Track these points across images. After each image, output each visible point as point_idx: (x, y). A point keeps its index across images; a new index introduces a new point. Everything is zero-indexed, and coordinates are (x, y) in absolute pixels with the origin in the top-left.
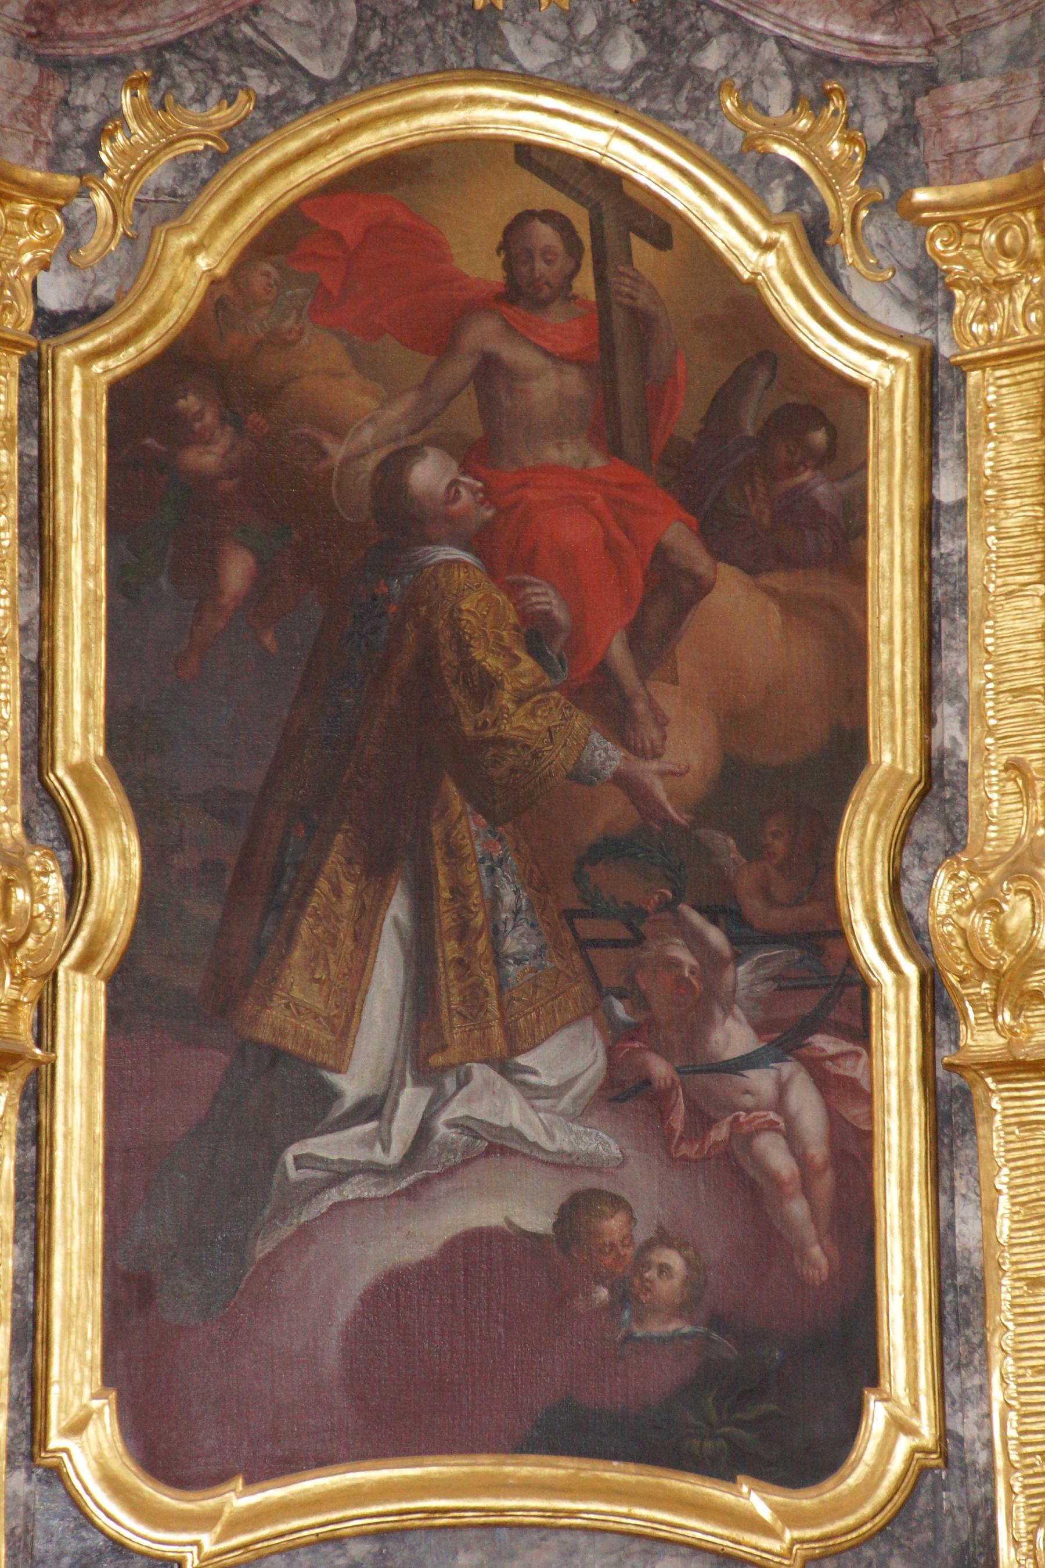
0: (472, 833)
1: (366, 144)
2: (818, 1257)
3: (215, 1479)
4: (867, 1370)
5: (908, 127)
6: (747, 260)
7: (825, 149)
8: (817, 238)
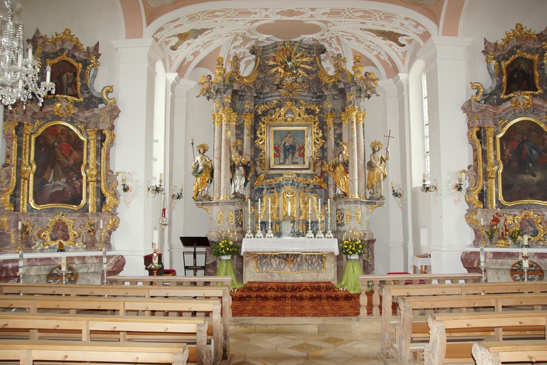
0: (58, 166)
1: (53, 124)
2: (79, 192)
3: (40, 205)
4: (82, 199)
5: (87, 126)
6: (77, 133)
7: (81, 127)
8: (81, 132)
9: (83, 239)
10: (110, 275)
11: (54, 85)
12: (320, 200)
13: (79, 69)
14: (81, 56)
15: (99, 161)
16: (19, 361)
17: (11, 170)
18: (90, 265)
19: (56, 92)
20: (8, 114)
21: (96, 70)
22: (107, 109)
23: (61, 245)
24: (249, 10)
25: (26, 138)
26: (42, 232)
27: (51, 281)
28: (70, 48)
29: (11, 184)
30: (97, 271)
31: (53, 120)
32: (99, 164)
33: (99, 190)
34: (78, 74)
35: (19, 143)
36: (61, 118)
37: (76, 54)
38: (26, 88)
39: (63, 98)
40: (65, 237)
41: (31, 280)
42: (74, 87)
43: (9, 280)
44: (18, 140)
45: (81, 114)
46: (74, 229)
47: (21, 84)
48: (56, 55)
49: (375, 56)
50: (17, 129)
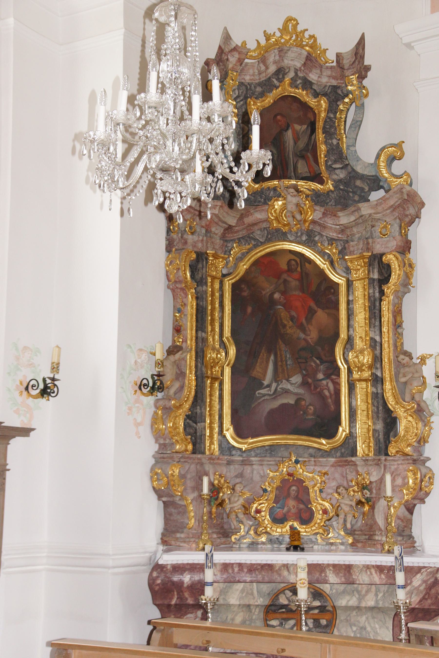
0: (281, 342)
1: (268, 250)
4: (338, 422)
5: (344, 248)
6: (322, 266)
8: (332, 263)
9: (345, 521)
10: (415, 620)
11: (269, 155)
13: (320, 112)
14: (324, 80)
15: (378, 332)
17: (184, 359)
18: (365, 588)
19: (273, 171)
20: (174, 236)
21: (361, 108)
22: (391, 202)
23: (295, 534)
25: (212, 286)
26: (253, 501)
27: (274, 623)
28: (298, 64)
29: (186, 391)
30: (381, 605)
31: (269, 240)
32: (378, 338)
33: (379, 402)
34: (320, 124)
35: (199, 298)
36: (285, 234)
37: (313, 77)
38: (211, 171)
39: (288, 187)
40: (305, 516)
41: (230, 616)
42: (311, 159)
43: (186, 614)
44: (197, 292)
45: (329, 222)
46: (324, 495)
47: (199, 166)
48: (267, 85)
50: (194, 269)
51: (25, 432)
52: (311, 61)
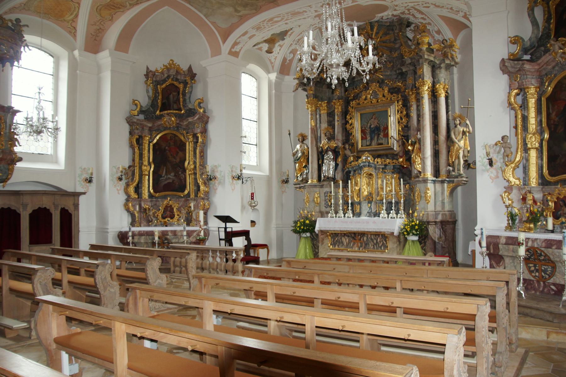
12: (402, 180)
16: (445, 345)
24: (296, 11)
34: (181, 92)
37: (179, 77)
48: (165, 81)
49: (463, 17)
51: (84, 193)
52: (178, 72)
